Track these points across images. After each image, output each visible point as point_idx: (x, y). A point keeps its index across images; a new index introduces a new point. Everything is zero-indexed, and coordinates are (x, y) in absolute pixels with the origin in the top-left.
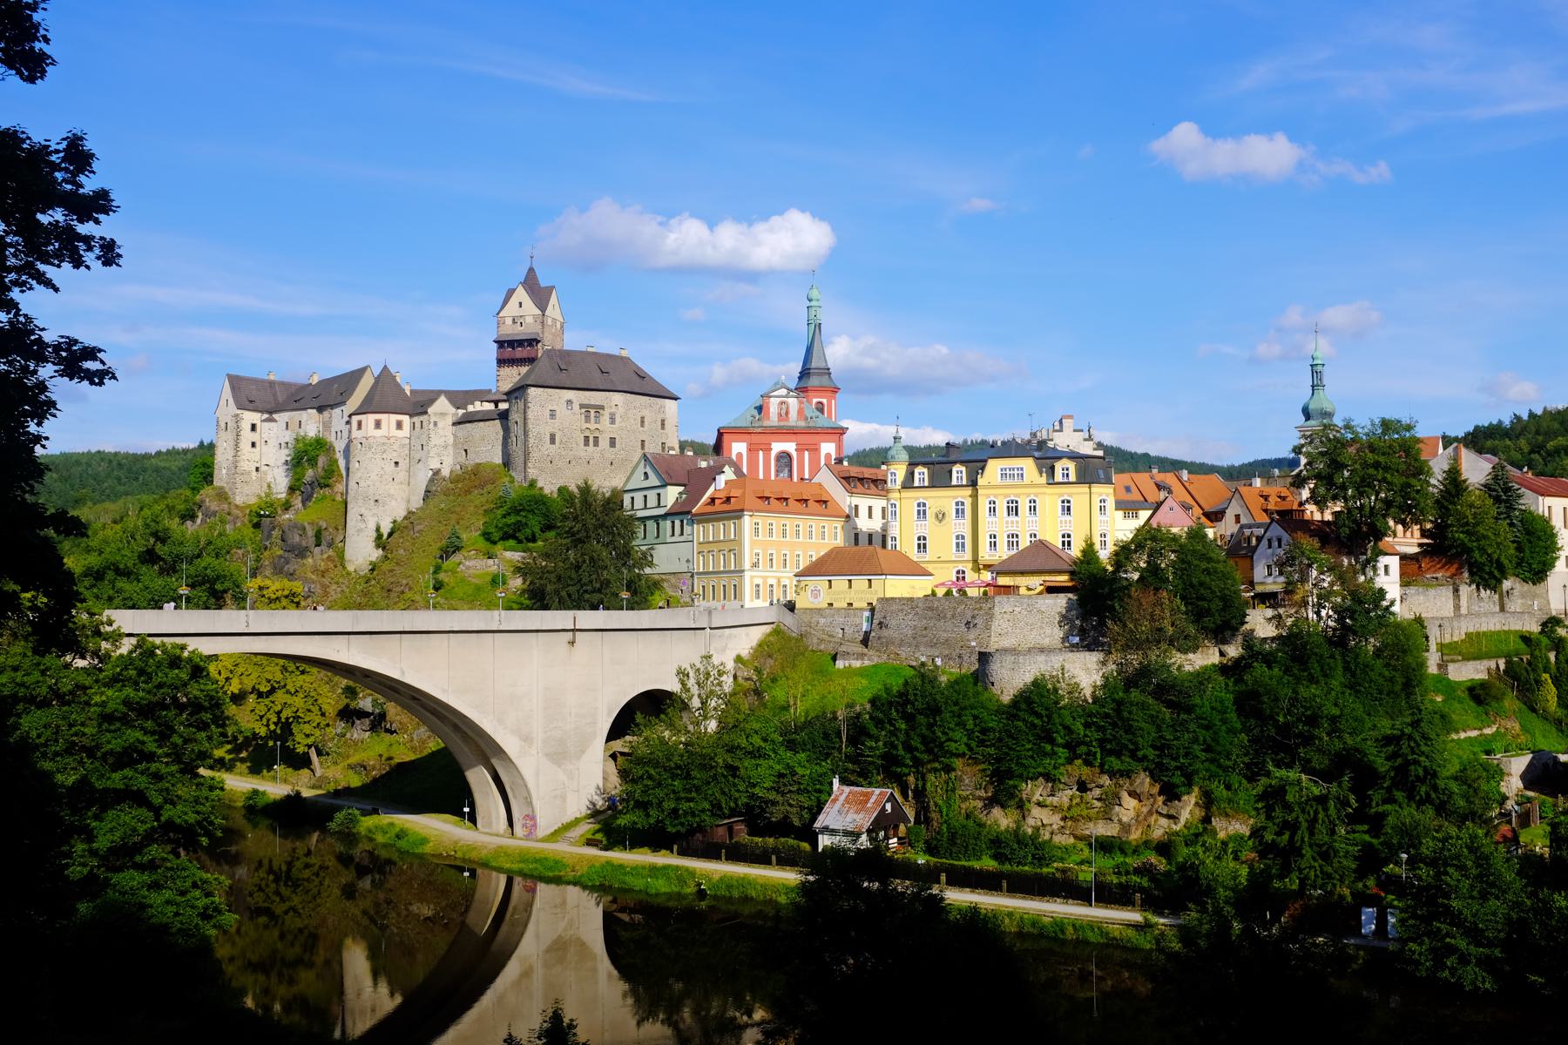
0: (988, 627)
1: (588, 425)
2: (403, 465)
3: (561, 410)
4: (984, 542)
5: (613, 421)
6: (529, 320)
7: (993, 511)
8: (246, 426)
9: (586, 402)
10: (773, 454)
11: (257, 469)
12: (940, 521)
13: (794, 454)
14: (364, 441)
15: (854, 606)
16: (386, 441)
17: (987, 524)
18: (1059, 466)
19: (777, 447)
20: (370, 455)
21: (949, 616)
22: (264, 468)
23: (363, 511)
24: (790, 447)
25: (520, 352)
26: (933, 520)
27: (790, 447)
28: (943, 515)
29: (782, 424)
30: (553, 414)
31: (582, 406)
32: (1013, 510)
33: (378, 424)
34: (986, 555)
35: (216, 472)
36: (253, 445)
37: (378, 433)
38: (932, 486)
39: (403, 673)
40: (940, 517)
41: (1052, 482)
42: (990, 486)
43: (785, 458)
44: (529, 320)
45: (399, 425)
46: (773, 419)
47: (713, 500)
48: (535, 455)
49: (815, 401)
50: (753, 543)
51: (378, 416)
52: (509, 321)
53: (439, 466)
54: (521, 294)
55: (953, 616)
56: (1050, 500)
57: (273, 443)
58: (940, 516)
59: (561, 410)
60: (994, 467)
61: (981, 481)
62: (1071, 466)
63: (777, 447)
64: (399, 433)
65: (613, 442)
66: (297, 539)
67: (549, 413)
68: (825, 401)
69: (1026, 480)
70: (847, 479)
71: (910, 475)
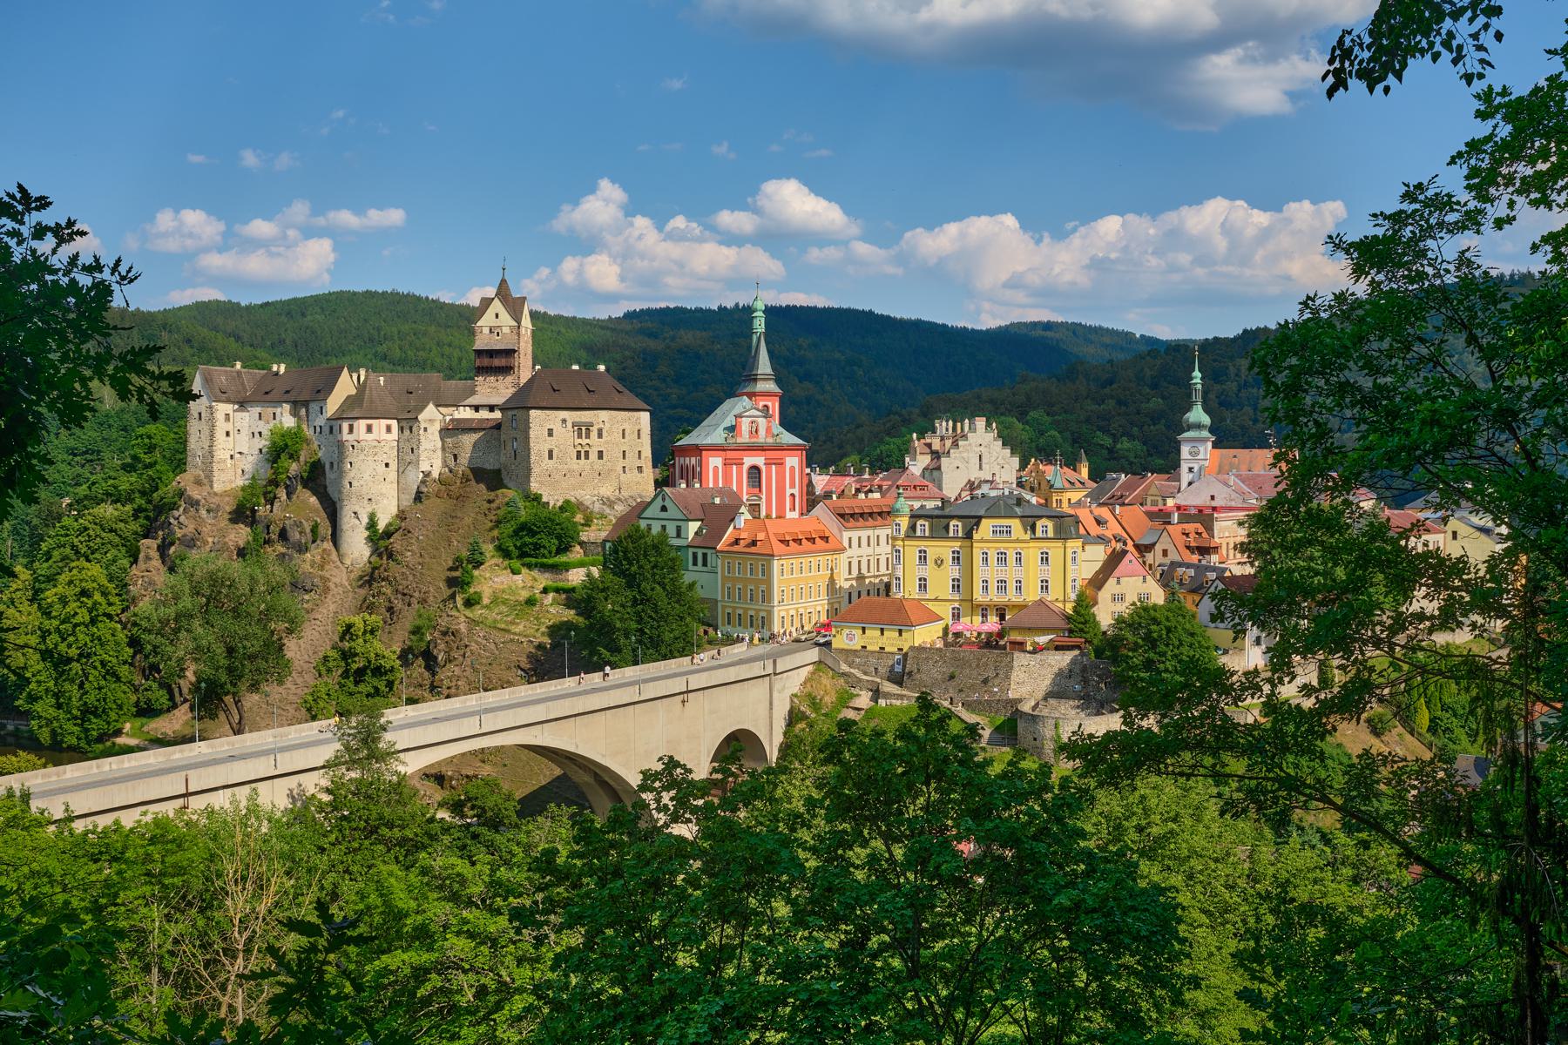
0: (1008, 677)
1: (580, 441)
2: (394, 466)
4: (978, 586)
5: (600, 435)
6: (506, 330)
8: (220, 416)
9: (578, 420)
10: (745, 468)
11: (232, 457)
13: (763, 468)
14: (355, 444)
15: (887, 650)
16: (376, 444)
17: (980, 572)
18: (1039, 524)
19: (749, 460)
20: (362, 457)
21: (974, 665)
23: (356, 509)
24: (759, 461)
25: (497, 362)
26: (933, 565)
27: (759, 461)
32: (1002, 558)
33: (369, 429)
34: (979, 596)
35: (189, 459)
36: (228, 434)
37: (370, 437)
38: (932, 537)
40: (939, 563)
42: (982, 541)
43: (755, 470)
44: (506, 330)
45: (389, 429)
46: (744, 437)
47: (737, 542)
48: (536, 470)
49: (762, 404)
50: (780, 581)
53: (429, 468)
54: (497, 306)
55: (978, 666)
56: (1032, 552)
57: (245, 433)
60: (987, 526)
61: (976, 536)
62: (1050, 524)
63: (749, 460)
65: (600, 455)
66: (297, 536)
68: (770, 404)
69: (1014, 537)
70: (842, 516)
71: (913, 528)
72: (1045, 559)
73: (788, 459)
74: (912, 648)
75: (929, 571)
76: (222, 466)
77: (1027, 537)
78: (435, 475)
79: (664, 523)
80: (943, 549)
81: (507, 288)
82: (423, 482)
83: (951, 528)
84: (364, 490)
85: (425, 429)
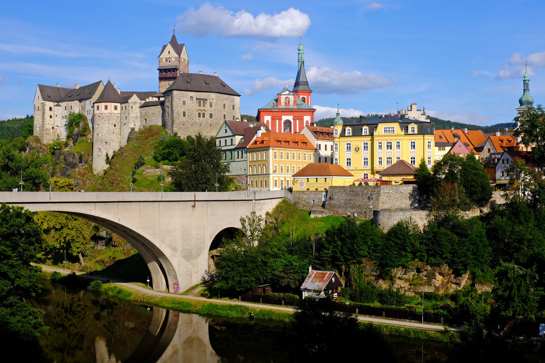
0: (378, 199)
1: (200, 108)
2: (118, 126)
3: (188, 101)
5: (211, 106)
6: (173, 59)
7: (380, 147)
8: (47, 108)
9: (199, 97)
10: (283, 121)
11: (53, 128)
12: (357, 152)
14: (100, 115)
15: (319, 190)
18: (410, 127)
19: (284, 118)
20: (103, 121)
21: (360, 194)
22: (56, 127)
23: (100, 147)
24: (290, 118)
25: (169, 74)
27: (290, 118)
28: (358, 149)
29: (287, 107)
30: (184, 103)
31: (197, 99)
32: (389, 146)
33: (106, 108)
35: (34, 129)
36: (51, 117)
37: (106, 111)
39: (119, 220)
40: (357, 150)
41: (407, 134)
42: (379, 136)
43: (288, 123)
44: (173, 59)
45: (116, 108)
46: (283, 105)
49: (301, 97)
50: (273, 161)
51: (106, 104)
52: (164, 60)
53: (133, 126)
54: (169, 48)
55: (362, 194)
56: (406, 142)
57: (59, 116)
58: (357, 149)
59: (188, 101)
60: (381, 127)
61: (375, 134)
62: (416, 126)
63: (284, 118)
64: (116, 112)
65: (211, 116)
66: (71, 160)
67: (182, 103)
68: (306, 97)
69: (395, 133)
71: (344, 131)
72: (413, 146)
73: (305, 117)
74: (330, 187)
75: (352, 154)
76: (47, 132)
77: (403, 133)
78: (137, 129)
79: (226, 139)
80: (358, 142)
81: (176, 40)
82: (130, 133)
83: (363, 131)
84: (104, 138)
85: (132, 107)
